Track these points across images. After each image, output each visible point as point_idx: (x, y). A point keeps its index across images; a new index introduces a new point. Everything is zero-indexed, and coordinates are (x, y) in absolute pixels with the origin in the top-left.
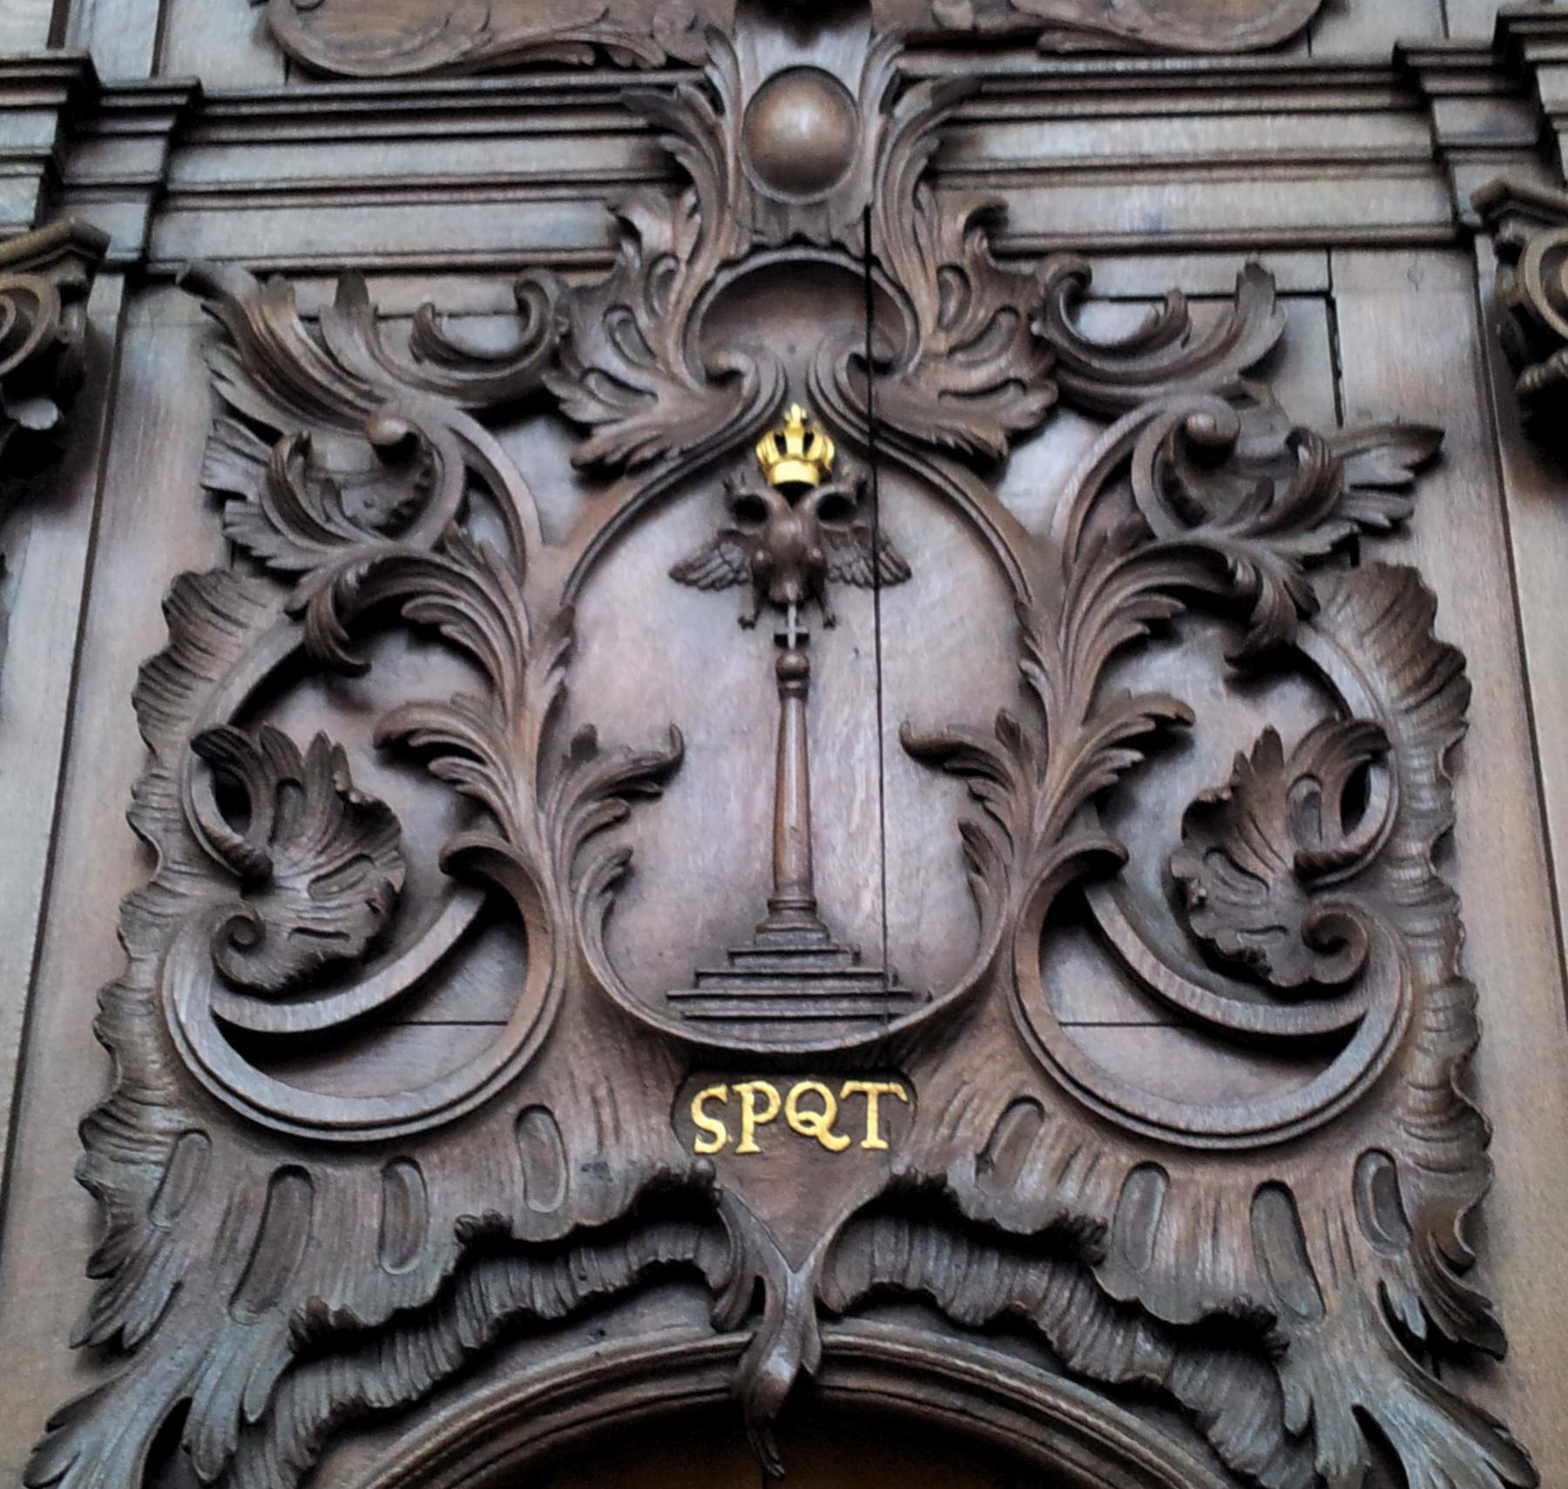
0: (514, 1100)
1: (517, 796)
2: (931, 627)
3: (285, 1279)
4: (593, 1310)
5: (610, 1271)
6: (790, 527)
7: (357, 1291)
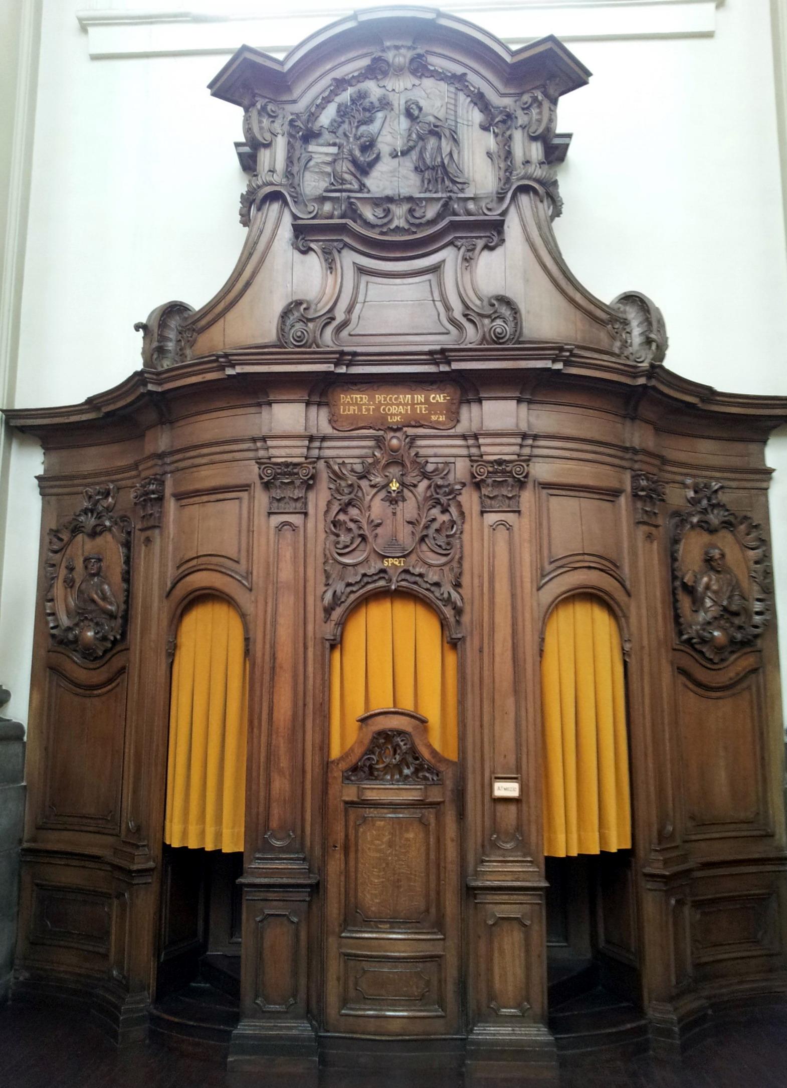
0: (366, 560)
1: (365, 526)
2: (409, 508)
3: (677, 551)
4: (375, 581)
5: (376, 578)
6: (394, 495)
7: (351, 580)
